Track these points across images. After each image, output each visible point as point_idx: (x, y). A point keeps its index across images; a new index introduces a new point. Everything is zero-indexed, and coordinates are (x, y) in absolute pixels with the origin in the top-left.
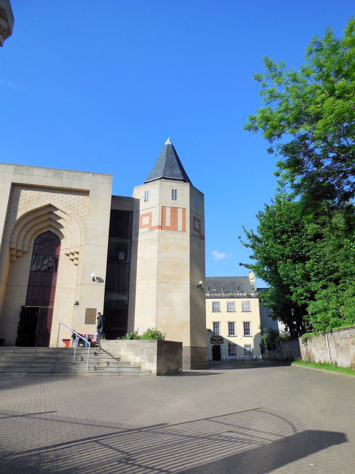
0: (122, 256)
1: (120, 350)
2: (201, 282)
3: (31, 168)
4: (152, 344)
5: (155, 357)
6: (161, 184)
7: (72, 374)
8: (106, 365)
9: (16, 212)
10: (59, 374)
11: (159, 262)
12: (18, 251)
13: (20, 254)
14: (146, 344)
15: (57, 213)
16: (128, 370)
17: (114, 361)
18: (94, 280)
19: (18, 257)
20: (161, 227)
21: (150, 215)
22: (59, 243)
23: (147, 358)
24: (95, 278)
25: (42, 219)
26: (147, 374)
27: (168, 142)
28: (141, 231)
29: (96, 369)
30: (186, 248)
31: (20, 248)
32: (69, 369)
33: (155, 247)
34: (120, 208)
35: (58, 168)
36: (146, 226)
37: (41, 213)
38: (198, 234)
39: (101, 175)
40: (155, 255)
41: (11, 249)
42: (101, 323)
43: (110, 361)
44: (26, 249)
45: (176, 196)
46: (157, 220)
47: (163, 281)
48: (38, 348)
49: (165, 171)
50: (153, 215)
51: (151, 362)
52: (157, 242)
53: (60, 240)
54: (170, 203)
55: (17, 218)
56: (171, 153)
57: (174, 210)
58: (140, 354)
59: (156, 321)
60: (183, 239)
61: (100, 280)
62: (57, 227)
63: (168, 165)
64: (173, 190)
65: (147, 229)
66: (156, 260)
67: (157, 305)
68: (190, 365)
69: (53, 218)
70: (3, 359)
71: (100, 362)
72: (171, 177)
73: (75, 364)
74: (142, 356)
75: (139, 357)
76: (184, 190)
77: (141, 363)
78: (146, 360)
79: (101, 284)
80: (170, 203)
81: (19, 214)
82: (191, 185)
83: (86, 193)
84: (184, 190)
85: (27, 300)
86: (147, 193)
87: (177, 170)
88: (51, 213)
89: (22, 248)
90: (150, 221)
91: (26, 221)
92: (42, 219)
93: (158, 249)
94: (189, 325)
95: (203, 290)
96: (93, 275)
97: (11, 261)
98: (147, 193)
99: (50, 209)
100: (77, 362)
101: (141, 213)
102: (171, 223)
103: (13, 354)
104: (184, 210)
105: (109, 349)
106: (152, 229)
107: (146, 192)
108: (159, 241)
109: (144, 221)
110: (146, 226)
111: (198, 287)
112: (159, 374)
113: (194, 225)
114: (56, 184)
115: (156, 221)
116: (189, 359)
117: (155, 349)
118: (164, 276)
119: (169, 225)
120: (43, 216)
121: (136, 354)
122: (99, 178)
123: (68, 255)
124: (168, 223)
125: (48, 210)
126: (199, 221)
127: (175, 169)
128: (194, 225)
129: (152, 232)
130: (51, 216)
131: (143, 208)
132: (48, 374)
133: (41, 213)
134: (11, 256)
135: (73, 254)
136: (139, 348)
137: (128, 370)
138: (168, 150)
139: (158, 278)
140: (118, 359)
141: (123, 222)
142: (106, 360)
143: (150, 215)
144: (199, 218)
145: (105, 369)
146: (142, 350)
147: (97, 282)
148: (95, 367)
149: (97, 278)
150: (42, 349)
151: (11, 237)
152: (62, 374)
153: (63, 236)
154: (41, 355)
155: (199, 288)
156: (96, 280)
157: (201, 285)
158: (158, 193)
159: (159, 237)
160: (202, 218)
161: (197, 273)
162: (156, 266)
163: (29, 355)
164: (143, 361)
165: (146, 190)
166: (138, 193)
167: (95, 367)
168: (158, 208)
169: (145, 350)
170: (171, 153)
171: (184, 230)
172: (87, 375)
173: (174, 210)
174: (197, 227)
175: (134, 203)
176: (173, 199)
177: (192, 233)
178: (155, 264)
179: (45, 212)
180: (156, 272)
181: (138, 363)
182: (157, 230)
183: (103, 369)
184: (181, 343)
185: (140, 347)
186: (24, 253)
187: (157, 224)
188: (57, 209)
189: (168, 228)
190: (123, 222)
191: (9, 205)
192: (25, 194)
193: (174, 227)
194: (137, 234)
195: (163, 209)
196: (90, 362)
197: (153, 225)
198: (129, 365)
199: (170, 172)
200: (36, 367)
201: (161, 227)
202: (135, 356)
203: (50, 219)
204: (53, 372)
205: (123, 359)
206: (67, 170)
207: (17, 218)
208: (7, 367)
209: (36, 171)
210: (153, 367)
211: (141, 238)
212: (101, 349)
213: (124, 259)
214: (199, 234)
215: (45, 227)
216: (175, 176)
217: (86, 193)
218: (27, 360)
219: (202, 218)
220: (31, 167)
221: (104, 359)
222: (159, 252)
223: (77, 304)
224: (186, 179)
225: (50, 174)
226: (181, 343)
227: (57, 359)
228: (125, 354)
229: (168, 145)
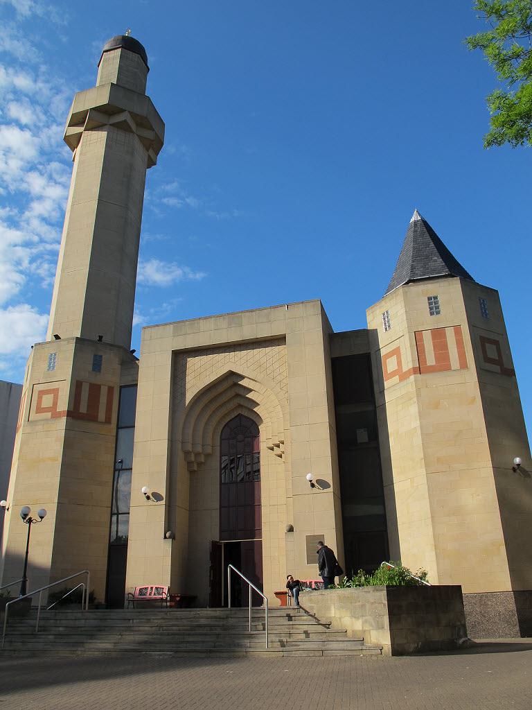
0: (362, 436)
1: (329, 609)
2: (518, 460)
3: (196, 321)
4: (378, 594)
5: (386, 620)
6: (405, 293)
7: (240, 654)
8: (303, 636)
9: (184, 394)
10: (218, 654)
11: (425, 436)
12: (197, 455)
13: (202, 459)
14: (369, 595)
15: (243, 383)
16: (341, 645)
17: (321, 628)
18: (313, 485)
19: (200, 464)
20: (419, 370)
21: (396, 352)
22: (256, 434)
23: (372, 621)
24: (314, 482)
25: (224, 398)
26: (373, 652)
27: (415, 217)
28: (387, 384)
29: (283, 646)
30: (474, 398)
31: (199, 449)
32: (239, 646)
33: (414, 409)
34: (337, 355)
35: (232, 315)
36: (393, 374)
37: (220, 389)
38: (497, 368)
39: (301, 305)
40: (416, 423)
41: (187, 453)
42: (324, 559)
43: (311, 629)
44: (209, 450)
45: (437, 308)
46: (410, 359)
47: (437, 468)
48: (200, 609)
49: (413, 268)
50: (402, 351)
51: (379, 628)
52: (415, 399)
53: (258, 427)
54: (429, 322)
55: (187, 402)
56: (422, 235)
57: (438, 334)
58: (360, 614)
59: (436, 547)
60: (465, 384)
61: (323, 484)
62: (249, 406)
63: (419, 255)
64: (429, 299)
65: (396, 378)
66: (419, 431)
67: (432, 517)
68: (518, 628)
69: (241, 392)
70: (146, 628)
71: (292, 631)
72: (424, 275)
73: (250, 636)
74: (364, 618)
75: (360, 621)
76: (451, 292)
77: (364, 631)
78: (371, 625)
79: (325, 490)
80: (429, 322)
81: (189, 397)
82: (466, 278)
83: (279, 340)
84: (451, 292)
85: (221, 531)
86: (386, 316)
87: (435, 261)
88: (236, 385)
89: (203, 449)
90: (399, 363)
91: (201, 405)
92: (224, 398)
93: (419, 412)
94: (503, 548)
95: (529, 475)
96: (309, 477)
97: (192, 472)
98: (386, 316)
99: (232, 378)
100: (252, 633)
101: (383, 352)
102: (437, 358)
103: (163, 621)
104: (457, 329)
105: (312, 608)
106: (404, 377)
107: (384, 314)
108: (418, 395)
109: (390, 365)
110: (393, 374)
111: (514, 470)
112: (397, 651)
113: (484, 352)
114: (234, 337)
115: (408, 362)
116: (514, 615)
117: (384, 605)
118: (438, 459)
119: (434, 363)
120: (225, 391)
121: (355, 616)
122: (299, 310)
123: (272, 449)
124: (431, 360)
125: (230, 382)
126: (496, 343)
127: (435, 257)
128: (484, 352)
129: (405, 382)
130: (237, 390)
131: (385, 342)
132: (203, 655)
133: (220, 389)
134: (189, 463)
135: (278, 446)
136: (357, 604)
137: (341, 645)
138: (415, 231)
139: (427, 466)
140: (327, 626)
141: (353, 377)
142: (305, 628)
143: (396, 352)
144: (493, 337)
145: (299, 646)
146: (363, 606)
147: (319, 489)
148: (281, 641)
149: (318, 481)
150: (206, 612)
151: (183, 434)
152: (225, 655)
153: (261, 420)
154: (203, 621)
155: (518, 471)
156: (316, 484)
157: (518, 465)
158: (403, 311)
159: (418, 390)
160: (503, 335)
161: (508, 442)
162: (420, 442)
163: (185, 622)
164: (367, 627)
165: (384, 310)
166: (373, 321)
167: (281, 641)
168: (407, 336)
169: (368, 606)
170: (422, 235)
171: (464, 365)
172: (265, 655)
173: (438, 334)
174: (492, 353)
175: (368, 337)
176: (432, 314)
177: (481, 369)
178: (418, 440)
179: (226, 385)
180: (422, 455)
181: (360, 631)
182: (412, 377)
183: (296, 645)
184: (460, 587)
185: (359, 602)
186: (208, 456)
187: (411, 366)
188: (242, 377)
189: (432, 370)
190: (353, 377)
191: (174, 385)
192: (193, 363)
193: (443, 364)
194: (382, 392)
195: (418, 336)
196: (269, 632)
197: (405, 369)
198: (346, 636)
199: (422, 267)
200: (188, 642)
201: (419, 370)
202: (354, 619)
203: (237, 395)
204: (211, 651)
205: (336, 625)
206: (247, 311)
207: (187, 402)
208: (146, 642)
209: (203, 325)
210: (382, 638)
211: (389, 397)
212: (301, 607)
213: (367, 441)
214: (505, 367)
215: (233, 410)
216: (433, 271)
217: (279, 340)
218: (179, 630)
219: (503, 335)
220: (195, 320)
221: (304, 623)
222: (421, 415)
223: (291, 529)
224: (454, 269)
225: (223, 323)
226: (460, 587)
227: (224, 628)
228: (337, 616)
229: (415, 222)
